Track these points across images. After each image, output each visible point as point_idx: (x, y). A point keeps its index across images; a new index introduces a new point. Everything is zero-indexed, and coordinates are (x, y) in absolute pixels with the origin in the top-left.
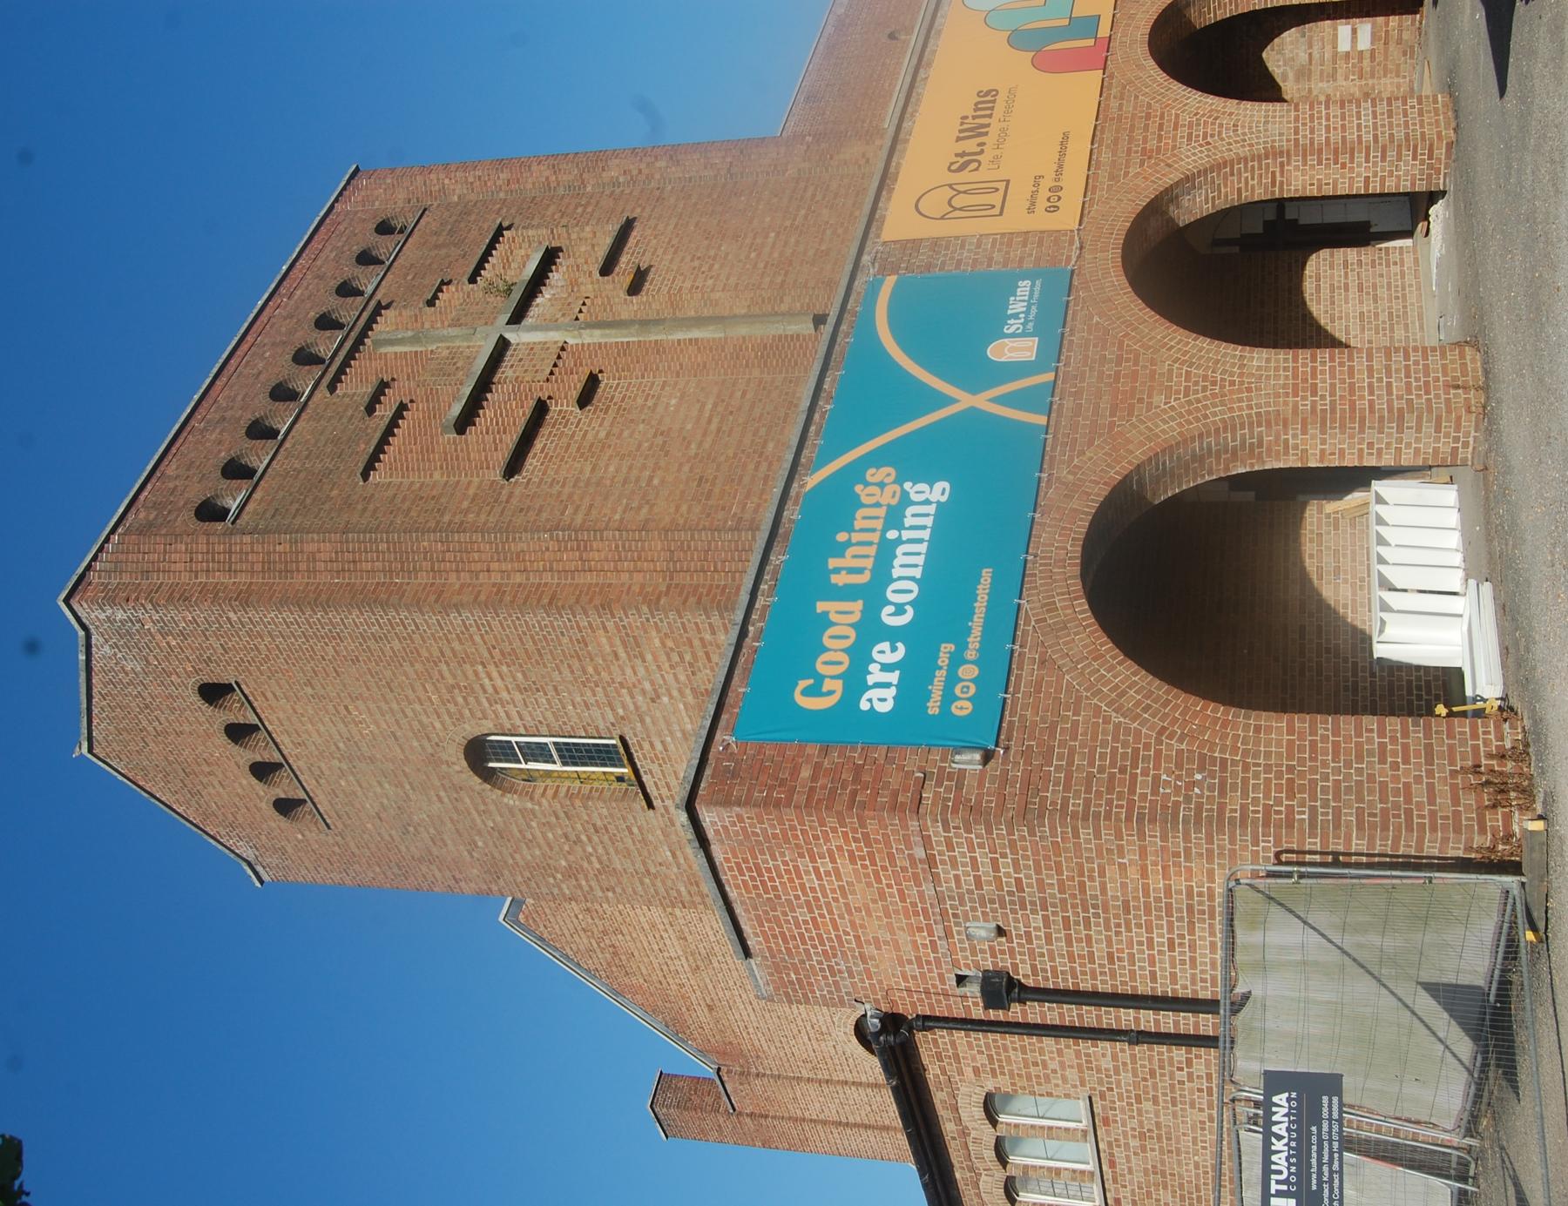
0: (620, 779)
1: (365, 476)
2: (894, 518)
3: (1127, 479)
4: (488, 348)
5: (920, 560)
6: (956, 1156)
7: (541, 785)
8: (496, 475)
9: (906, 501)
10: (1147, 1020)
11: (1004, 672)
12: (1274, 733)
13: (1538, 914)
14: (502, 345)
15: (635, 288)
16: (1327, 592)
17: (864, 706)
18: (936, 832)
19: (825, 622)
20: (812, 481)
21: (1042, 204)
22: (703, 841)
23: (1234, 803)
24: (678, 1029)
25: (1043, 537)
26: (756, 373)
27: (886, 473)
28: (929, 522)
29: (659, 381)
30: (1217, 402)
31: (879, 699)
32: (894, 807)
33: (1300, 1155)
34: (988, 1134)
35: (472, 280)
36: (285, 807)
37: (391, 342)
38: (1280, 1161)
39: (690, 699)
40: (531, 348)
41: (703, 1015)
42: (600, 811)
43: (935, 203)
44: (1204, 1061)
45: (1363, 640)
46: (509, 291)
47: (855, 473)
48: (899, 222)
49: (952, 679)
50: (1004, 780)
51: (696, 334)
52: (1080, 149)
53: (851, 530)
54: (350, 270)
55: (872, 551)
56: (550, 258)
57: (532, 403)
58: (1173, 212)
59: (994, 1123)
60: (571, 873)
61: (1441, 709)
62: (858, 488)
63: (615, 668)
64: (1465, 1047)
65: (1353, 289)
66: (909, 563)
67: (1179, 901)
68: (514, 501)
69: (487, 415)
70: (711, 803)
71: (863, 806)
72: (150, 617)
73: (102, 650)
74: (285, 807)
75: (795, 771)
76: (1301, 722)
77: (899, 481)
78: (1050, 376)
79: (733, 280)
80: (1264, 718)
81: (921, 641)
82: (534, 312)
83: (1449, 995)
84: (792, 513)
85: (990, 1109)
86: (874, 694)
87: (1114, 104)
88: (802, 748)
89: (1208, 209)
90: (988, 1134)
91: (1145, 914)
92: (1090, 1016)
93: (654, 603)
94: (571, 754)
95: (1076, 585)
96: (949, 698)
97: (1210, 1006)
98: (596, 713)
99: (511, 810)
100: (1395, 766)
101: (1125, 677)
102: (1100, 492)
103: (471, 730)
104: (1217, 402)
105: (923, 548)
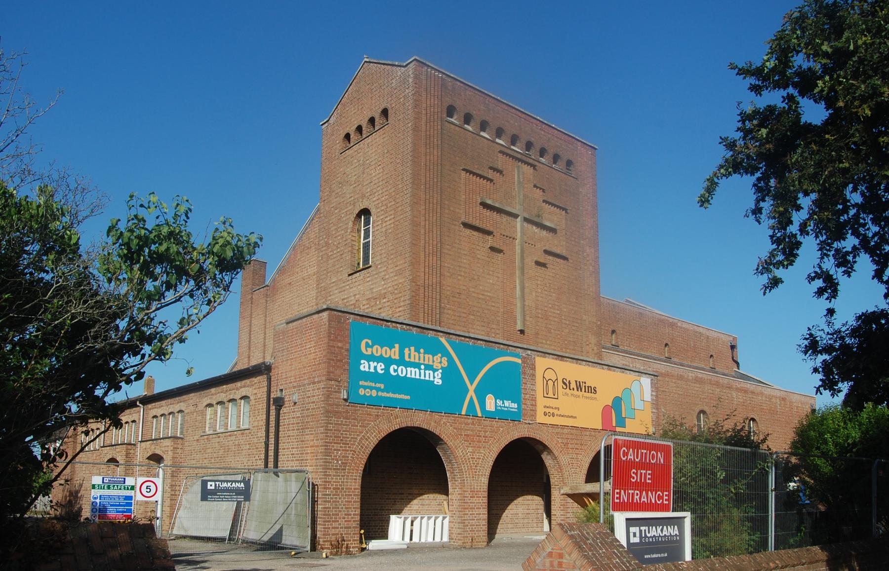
0: (359, 264)
1: (464, 170)
2: (428, 367)
3: (442, 440)
5: (413, 376)
7: (356, 235)
8: (463, 219)
9: (435, 371)
10: (272, 447)
12: (354, 483)
13: (299, 555)
14: (516, 216)
15: (538, 263)
16: (415, 502)
17: (362, 361)
18: (322, 385)
19: (391, 347)
20: (443, 340)
21: (547, 410)
22: (319, 312)
23: (332, 473)
24: (282, 271)
26: (502, 310)
27: (445, 363)
28: (427, 378)
29: (500, 275)
30: (470, 466)
31: (364, 366)
33: (227, 490)
35: (544, 201)
36: (347, 137)
37: (519, 172)
38: (225, 485)
39: (383, 292)
40: (515, 227)
41: (288, 280)
42: (347, 256)
43: (550, 375)
44: (261, 464)
45: (398, 512)
46: (539, 216)
47: (446, 353)
48: (542, 363)
49: (371, 388)
50: (338, 405)
52: (570, 422)
53: (424, 353)
54: (551, 152)
55: (417, 361)
56: (552, 230)
57: (491, 229)
58: (545, 453)
59: (241, 398)
60: (327, 244)
61: (362, 531)
62: (440, 355)
63: (392, 266)
64: (266, 539)
66: (412, 373)
67: (305, 457)
70: (329, 315)
71: (329, 363)
72: (409, 92)
73: (399, 71)
74: (347, 137)
75: (340, 341)
77: (442, 368)
78: (480, 415)
79: (540, 299)
80: (359, 481)
81: (386, 378)
82: (530, 226)
83: (280, 532)
84: (431, 334)
85: (245, 398)
87: (588, 433)
89: (547, 464)
91: (302, 449)
92: (272, 430)
93: (413, 281)
94: (366, 246)
95: (404, 425)
96: (365, 387)
98: (378, 258)
100: (344, 518)
101: (373, 441)
102: (437, 432)
103: (373, 211)
104: (470, 466)
105: (418, 377)
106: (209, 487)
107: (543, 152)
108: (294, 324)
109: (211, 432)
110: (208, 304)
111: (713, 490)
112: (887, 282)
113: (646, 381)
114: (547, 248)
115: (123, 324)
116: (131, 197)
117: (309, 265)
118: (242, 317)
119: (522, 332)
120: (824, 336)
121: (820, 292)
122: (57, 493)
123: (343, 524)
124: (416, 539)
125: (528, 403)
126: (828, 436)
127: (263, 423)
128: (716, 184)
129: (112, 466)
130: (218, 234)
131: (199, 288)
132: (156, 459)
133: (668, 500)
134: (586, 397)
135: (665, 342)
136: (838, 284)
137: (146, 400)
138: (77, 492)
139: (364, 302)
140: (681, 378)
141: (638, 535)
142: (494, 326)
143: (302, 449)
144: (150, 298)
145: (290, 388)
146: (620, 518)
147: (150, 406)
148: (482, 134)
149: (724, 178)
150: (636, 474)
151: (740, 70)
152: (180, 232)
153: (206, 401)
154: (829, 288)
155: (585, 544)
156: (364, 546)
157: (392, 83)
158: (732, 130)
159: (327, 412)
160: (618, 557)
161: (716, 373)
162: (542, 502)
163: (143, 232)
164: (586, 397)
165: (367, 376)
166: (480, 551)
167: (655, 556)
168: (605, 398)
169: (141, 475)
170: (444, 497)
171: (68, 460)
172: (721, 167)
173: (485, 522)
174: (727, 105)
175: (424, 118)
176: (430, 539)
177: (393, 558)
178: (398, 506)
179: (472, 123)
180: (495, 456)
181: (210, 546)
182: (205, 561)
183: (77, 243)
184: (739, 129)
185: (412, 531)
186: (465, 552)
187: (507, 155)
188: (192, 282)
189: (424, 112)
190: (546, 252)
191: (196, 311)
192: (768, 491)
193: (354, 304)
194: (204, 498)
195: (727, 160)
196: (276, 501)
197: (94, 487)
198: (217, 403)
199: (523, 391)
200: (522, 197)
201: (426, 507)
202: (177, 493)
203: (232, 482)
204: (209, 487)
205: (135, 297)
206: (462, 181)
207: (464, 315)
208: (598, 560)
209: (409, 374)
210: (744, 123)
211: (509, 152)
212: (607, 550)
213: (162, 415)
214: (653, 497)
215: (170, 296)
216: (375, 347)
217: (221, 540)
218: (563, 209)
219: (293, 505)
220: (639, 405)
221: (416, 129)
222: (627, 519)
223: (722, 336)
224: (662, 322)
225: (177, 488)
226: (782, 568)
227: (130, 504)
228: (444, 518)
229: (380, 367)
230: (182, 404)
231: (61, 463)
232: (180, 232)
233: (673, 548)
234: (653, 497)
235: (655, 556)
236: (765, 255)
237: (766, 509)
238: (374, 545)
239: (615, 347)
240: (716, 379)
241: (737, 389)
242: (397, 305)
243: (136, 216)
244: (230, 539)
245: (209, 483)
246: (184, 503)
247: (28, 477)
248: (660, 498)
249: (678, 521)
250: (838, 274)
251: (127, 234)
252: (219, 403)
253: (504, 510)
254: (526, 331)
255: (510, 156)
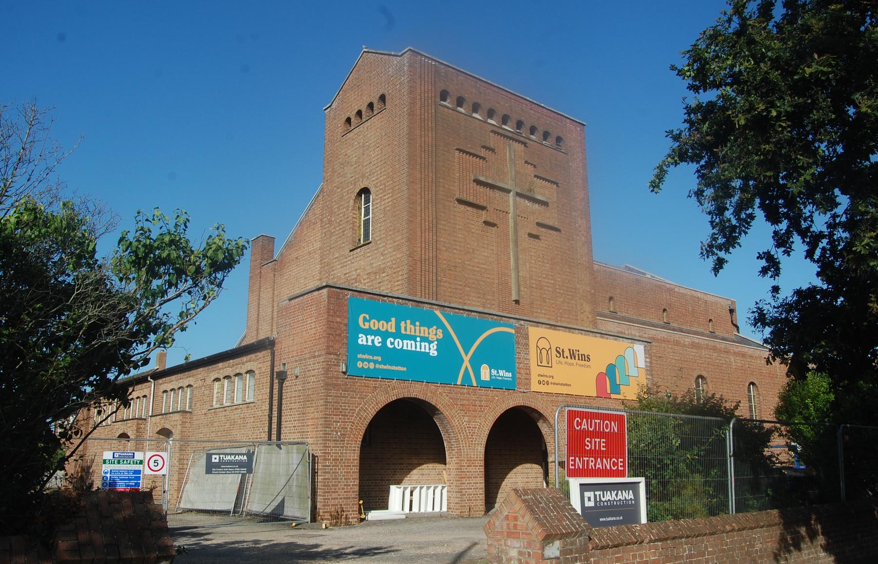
0: (360, 240)
1: (457, 149)
2: (424, 339)
4: (506, 187)
5: (409, 348)
6: (237, 360)
8: (457, 196)
9: (430, 342)
10: (275, 420)
11: (371, 376)
12: (353, 454)
14: (509, 191)
15: (531, 235)
16: (415, 471)
17: (360, 335)
18: (322, 359)
20: (438, 313)
21: (542, 379)
22: (319, 289)
24: (289, 245)
25: (418, 385)
28: (423, 350)
29: (494, 248)
31: (362, 340)
32: (328, 347)
33: (230, 463)
34: (243, 371)
35: (535, 176)
36: (348, 120)
38: (228, 458)
41: (294, 255)
43: (543, 344)
44: (265, 436)
45: (398, 482)
48: (534, 332)
49: (369, 361)
50: (337, 378)
51: (512, 259)
54: (541, 130)
55: (413, 333)
56: (544, 204)
57: (485, 205)
59: (247, 373)
60: (330, 221)
61: (361, 502)
64: (269, 510)
65: (527, 480)
66: (408, 345)
67: (306, 429)
68: (447, 203)
69: (481, 189)
70: (328, 292)
71: (328, 337)
72: (405, 79)
73: (396, 60)
74: (348, 120)
75: (339, 317)
76: (357, 463)
78: (475, 385)
80: (358, 452)
81: (382, 351)
82: (522, 200)
85: (250, 372)
86: (364, 338)
88: (347, 318)
89: (543, 432)
90: (243, 371)
91: (303, 424)
93: (410, 256)
94: (367, 222)
95: (401, 396)
96: (363, 360)
97: (279, 438)
98: (378, 233)
99: (349, 202)
100: (343, 489)
101: (371, 412)
103: (372, 190)
104: (467, 435)
105: (414, 349)
106: (213, 460)
107: (533, 130)
108: (296, 300)
109: (218, 406)
110: (204, 299)
111: (670, 456)
112: (817, 261)
113: (639, 348)
114: (540, 221)
115: (131, 317)
116: (139, 213)
117: (314, 241)
118: (251, 291)
119: (517, 302)
120: (771, 310)
121: (764, 271)
122: (71, 467)
123: (342, 494)
124: (415, 509)
125: (522, 371)
126: (808, 401)
127: (267, 396)
128: (666, 172)
129: (123, 441)
130: (211, 241)
131: (197, 285)
132: (166, 433)
133: (623, 466)
134: (580, 365)
135: (663, 307)
136: (779, 263)
137: (157, 376)
138: (89, 467)
139: (365, 277)
140: (677, 343)
141: (592, 499)
142: (490, 297)
143: (303, 424)
144: (154, 295)
145: (292, 362)
146: (574, 484)
147: (160, 381)
148: (475, 115)
149: (672, 167)
150: (591, 442)
151: (679, 71)
152: (180, 239)
153: (214, 375)
154: (771, 266)
155: (538, 507)
156: (363, 516)
157: (387, 71)
158: (679, 124)
159: (327, 384)
160: (568, 519)
161: (716, 337)
162: (541, 471)
163: (148, 242)
164: (580, 365)
165: (365, 349)
166: (476, 521)
167: (610, 519)
168: (599, 366)
169: (150, 450)
170: (442, 466)
171: (83, 437)
172: (669, 156)
173: (482, 491)
174: (671, 104)
175: (419, 103)
176: (430, 509)
177: (390, 528)
178: (397, 477)
179: (465, 105)
180: (490, 425)
181: (215, 519)
182: (209, 534)
183: (94, 249)
184: (685, 121)
185: (411, 501)
186: (462, 521)
187: (499, 134)
188: (190, 282)
189: (418, 97)
190: (538, 224)
191: (193, 306)
192: (726, 457)
193: (355, 279)
194: (209, 471)
195: (673, 150)
196: (278, 474)
197: (105, 462)
198: (224, 378)
199: (517, 360)
200: (513, 173)
201: (425, 477)
202: (185, 467)
203: (236, 454)
204: (213, 460)
205: (142, 296)
206: (456, 160)
207: (460, 287)
208: (548, 522)
209: (405, 346)
210: (689, 116)
211: (500, 131)
212: (558, 513)
213: (171, 390)
214: (607, 464)
215: (172, 292)
216: (372, 321)
217: (226, 513)
218: (554, 183)
219: (294, 476)
220: (633, 371)
221: (411, 114)
222: (581, 485)
223: (720, 300)
224: (660, 288)
225: (185, 462)
226: (739, 530)
227: (139, 478)
228: (443, 488)
229: (378, 341)
230: (191, 379)
231: (76, 441)
232: (180, 239)
233: (629, 512)
234: (607, 464)
235: (610, 519)
236: (707, 240)
237: (725, 473)
238: (374, 515)
239: (613, 315)
240: (713, 344)
241: (735, 354)
242: (396, 279)
243: (142, 229)
244: (235, 512)
245: (214, 456)
246: (191, 476)
247: (46, 453)
248: (615, 464)
249: (634, 486)
250: (778, 253)
251: (135, 244)
252: (226, 377)
253: (503, 479)
254: (521, 301)
255: (502, 135)
